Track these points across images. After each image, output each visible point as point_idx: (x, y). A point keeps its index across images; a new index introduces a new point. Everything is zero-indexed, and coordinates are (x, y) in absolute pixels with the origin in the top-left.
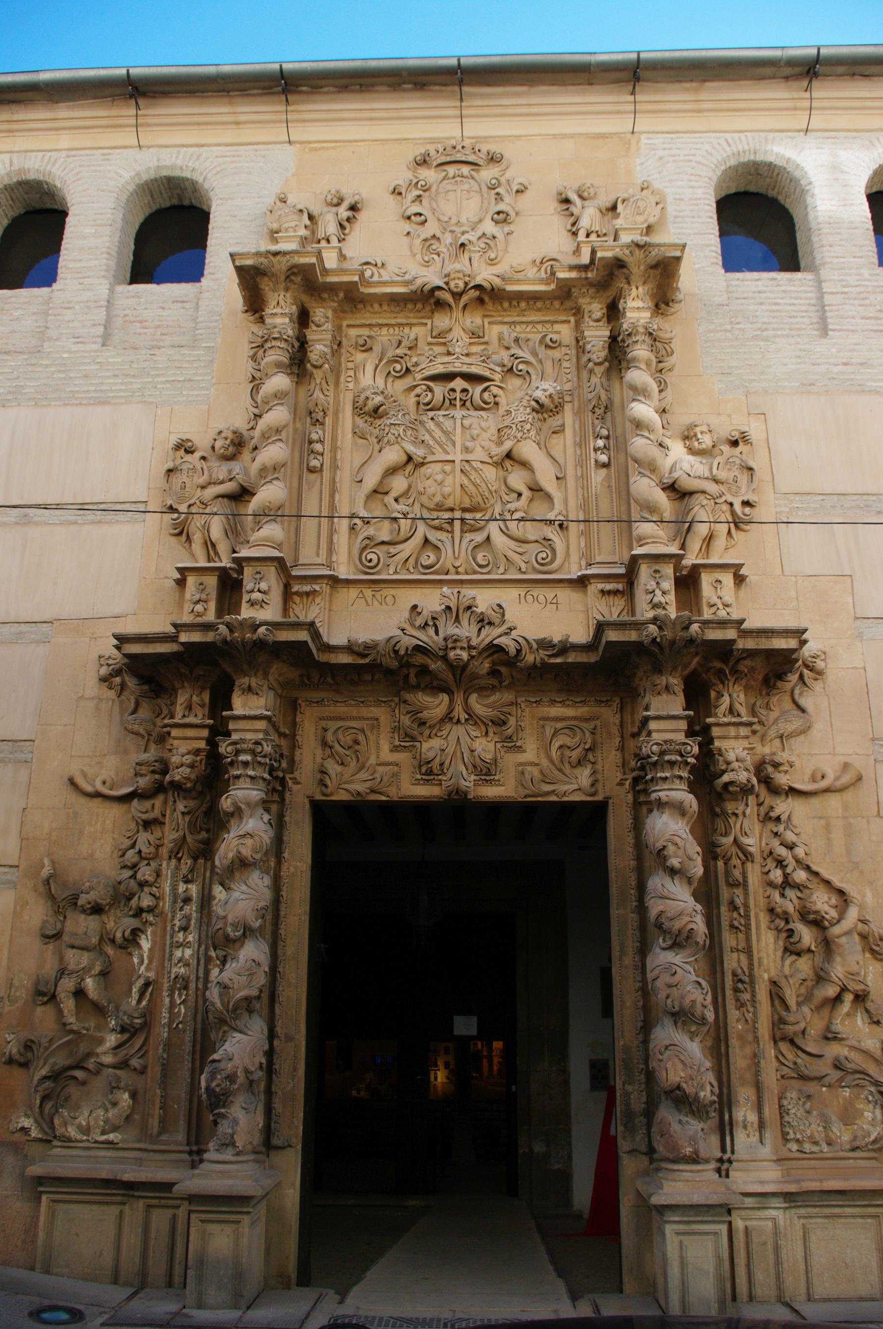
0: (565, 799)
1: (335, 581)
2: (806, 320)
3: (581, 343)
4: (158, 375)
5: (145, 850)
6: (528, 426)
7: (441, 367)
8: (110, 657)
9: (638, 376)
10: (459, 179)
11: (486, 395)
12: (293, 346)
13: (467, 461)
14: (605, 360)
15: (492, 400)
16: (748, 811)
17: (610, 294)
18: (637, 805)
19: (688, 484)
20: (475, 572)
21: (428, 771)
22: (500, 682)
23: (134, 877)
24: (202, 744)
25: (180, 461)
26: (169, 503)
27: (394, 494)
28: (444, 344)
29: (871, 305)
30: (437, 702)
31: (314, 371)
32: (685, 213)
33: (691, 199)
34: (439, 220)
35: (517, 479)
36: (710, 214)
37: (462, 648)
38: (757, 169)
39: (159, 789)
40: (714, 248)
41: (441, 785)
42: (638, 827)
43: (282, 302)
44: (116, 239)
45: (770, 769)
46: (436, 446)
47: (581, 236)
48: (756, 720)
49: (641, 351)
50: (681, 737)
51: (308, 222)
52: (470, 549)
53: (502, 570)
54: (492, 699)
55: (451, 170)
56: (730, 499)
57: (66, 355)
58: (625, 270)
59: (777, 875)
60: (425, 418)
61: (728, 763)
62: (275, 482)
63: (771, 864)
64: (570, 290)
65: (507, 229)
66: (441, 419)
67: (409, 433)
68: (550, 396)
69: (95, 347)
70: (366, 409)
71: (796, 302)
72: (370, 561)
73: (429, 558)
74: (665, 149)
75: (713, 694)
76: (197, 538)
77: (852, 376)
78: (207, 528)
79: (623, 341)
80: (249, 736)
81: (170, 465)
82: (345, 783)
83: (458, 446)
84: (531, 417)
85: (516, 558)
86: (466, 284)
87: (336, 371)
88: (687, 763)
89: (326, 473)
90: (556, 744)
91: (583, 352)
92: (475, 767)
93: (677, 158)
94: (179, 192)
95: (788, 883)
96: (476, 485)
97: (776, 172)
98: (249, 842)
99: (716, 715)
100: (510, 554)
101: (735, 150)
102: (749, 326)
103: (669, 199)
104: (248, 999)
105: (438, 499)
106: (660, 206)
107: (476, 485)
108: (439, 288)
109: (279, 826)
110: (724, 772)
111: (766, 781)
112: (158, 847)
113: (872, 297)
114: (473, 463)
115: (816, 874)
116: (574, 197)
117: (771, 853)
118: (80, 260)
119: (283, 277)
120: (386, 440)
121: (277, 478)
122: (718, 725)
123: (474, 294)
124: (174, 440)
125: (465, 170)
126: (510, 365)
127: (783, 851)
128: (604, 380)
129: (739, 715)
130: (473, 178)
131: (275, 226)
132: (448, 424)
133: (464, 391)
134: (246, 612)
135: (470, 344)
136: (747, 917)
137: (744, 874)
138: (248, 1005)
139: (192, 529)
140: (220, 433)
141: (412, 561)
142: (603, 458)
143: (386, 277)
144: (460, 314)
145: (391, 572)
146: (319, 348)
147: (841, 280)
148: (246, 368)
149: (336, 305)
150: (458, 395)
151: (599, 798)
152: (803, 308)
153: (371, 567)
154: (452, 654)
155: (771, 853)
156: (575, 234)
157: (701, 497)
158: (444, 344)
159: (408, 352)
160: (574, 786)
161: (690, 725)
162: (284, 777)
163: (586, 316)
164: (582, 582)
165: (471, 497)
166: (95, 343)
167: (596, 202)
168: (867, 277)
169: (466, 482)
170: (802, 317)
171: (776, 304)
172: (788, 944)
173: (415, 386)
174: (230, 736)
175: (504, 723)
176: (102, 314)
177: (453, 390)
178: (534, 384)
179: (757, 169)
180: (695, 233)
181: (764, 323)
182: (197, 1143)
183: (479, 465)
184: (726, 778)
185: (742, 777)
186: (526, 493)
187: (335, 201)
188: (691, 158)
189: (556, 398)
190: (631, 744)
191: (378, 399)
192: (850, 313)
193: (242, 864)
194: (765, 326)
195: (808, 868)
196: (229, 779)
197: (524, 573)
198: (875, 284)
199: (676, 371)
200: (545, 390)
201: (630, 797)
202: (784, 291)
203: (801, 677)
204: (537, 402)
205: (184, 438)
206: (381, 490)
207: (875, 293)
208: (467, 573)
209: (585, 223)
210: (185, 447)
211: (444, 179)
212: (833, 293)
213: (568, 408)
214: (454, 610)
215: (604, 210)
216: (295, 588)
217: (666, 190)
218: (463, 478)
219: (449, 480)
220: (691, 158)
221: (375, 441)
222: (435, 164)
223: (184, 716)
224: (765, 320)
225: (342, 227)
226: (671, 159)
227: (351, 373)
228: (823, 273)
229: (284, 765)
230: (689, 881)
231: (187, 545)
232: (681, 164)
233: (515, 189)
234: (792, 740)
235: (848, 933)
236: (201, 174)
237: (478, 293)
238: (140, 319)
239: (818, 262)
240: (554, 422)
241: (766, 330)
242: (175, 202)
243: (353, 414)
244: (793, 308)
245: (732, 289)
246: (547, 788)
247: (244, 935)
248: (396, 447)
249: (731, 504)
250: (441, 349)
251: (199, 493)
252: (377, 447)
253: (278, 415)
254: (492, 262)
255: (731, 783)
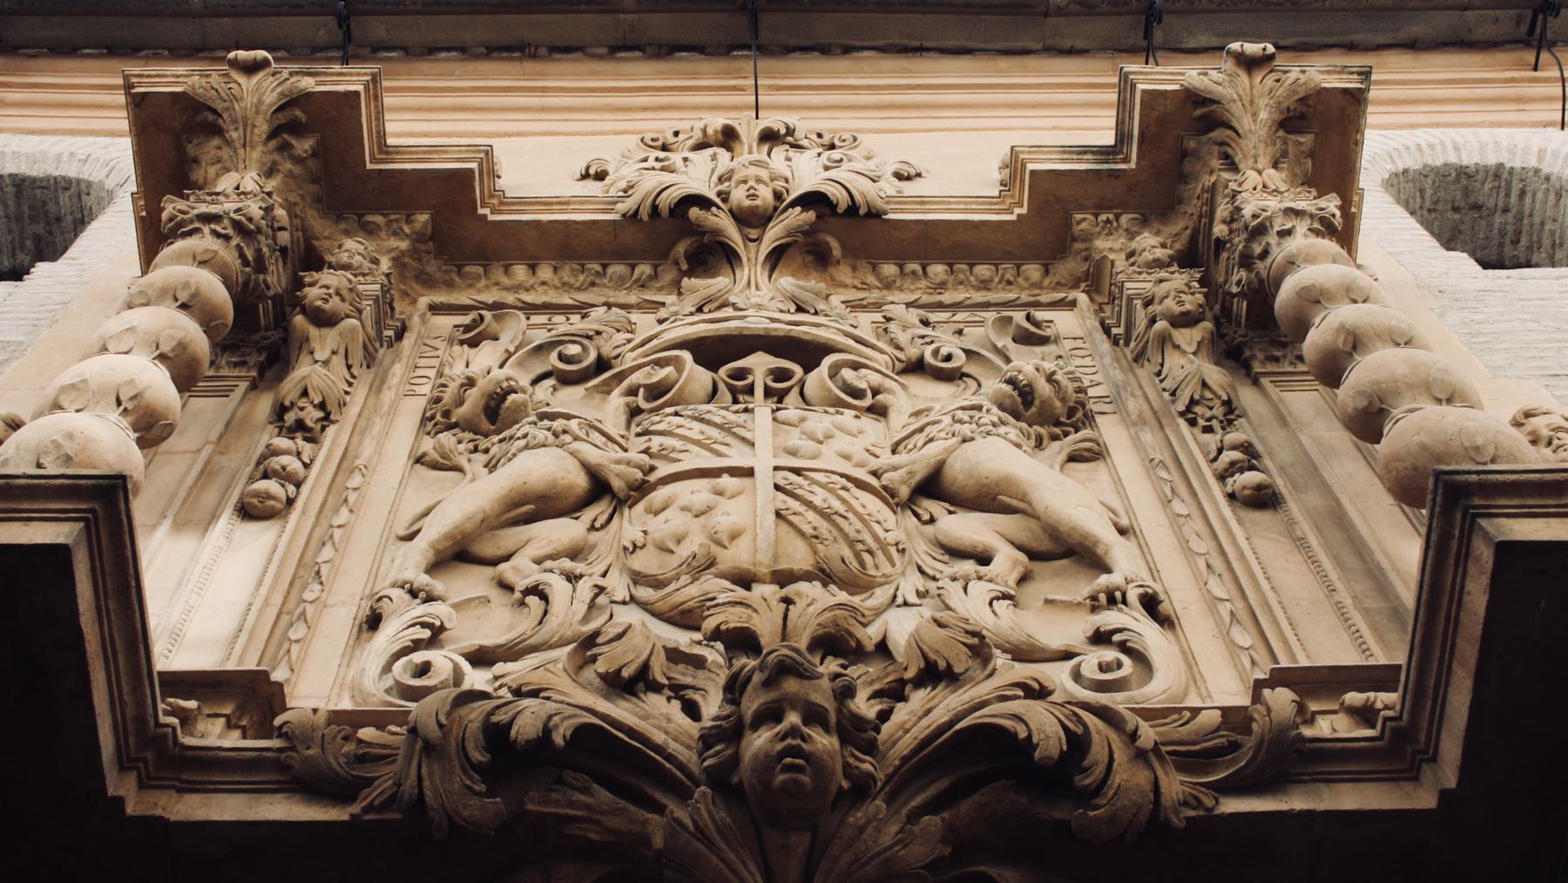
31: (313, 332)
38: (1467, 192)
58: (1220, 134)
86: (778, 196)
94: (40, 229)
97: (1516, 187)
105: (694, 544)
119: (262, 128)
123: (797, 217)
144: (761, 276)
149: (404, 245)
165: (813, 539)
179: (1467, 192)
237: (811, 215)
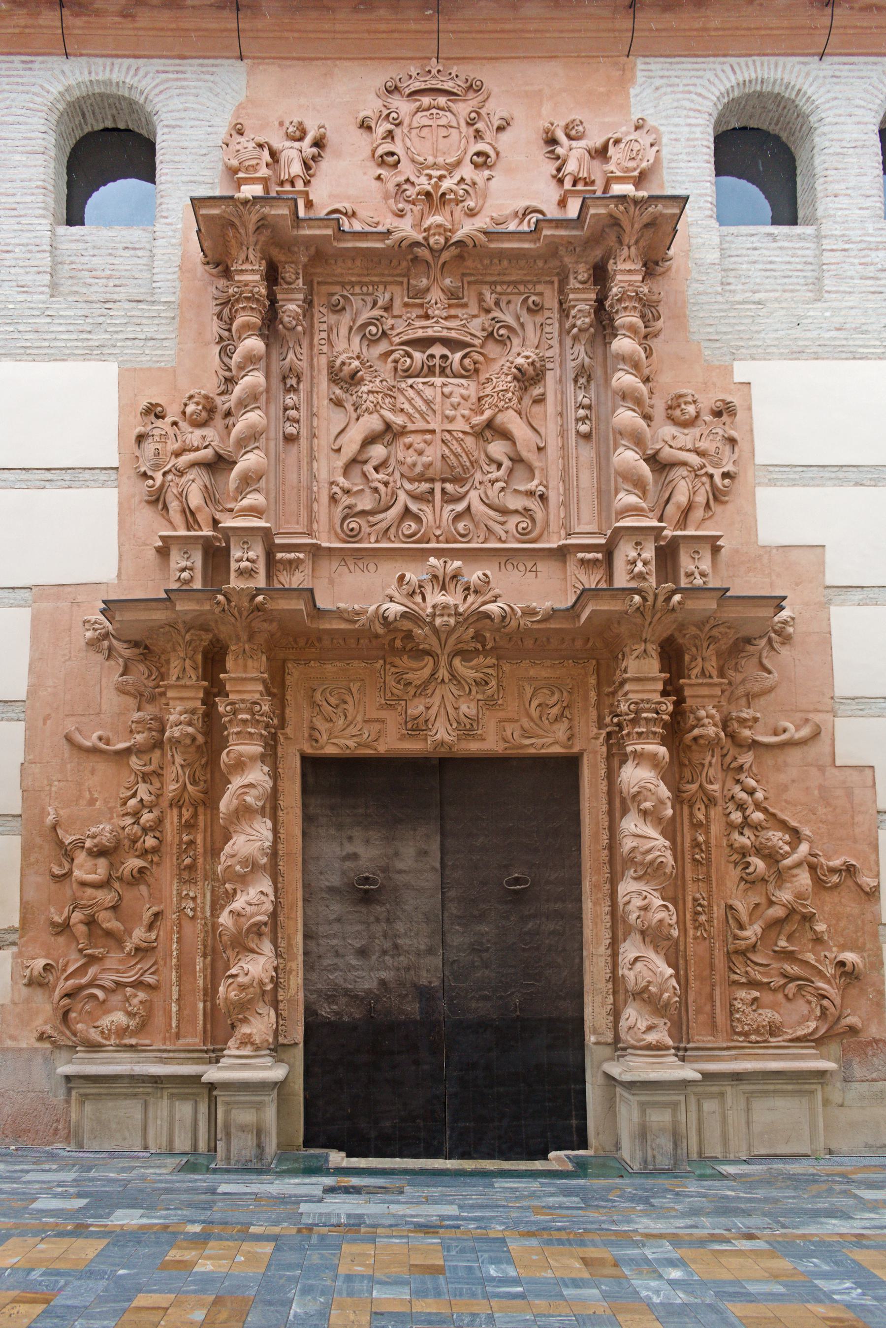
0: (543, 751)
1: (316, 551)
2: (802, 281)
3: (564, 306)
4: (117, 332)
5: (146, 798)
6: (510, 395)
7: (420, 331)
8: (96, 622)
9: (623, 344)
10: (434, 111)
11: (467, 361)
12: (264, 306)
13: (449, 431)
14: (591, 326)
15: (472, 367)
16: (714, 761)
17: (597, 254)
18: (610, 756)
19: (667, 453)
20: (456, 542)
21: (417, 728)
22: (484, 646)
23: (137, 822)
24: (198, 704)
25: (151, 427)
26: (142, 469)
27: (374, 462)
28: (421, 306)
29: (872, 264)
30: (422, 664)
32: (680, 157)
33: (688, 140)
34: (413, 161)
35: (497, 449)
36: (707, 157)
37: (449, 615)
39: (158, 744)
40: (710, 199)
41: (426, 739)
42: (611, 776)
43: (251, 257)
44: (51, 171)
45: (736, 725)
46: (417, 415)
47: (568, 185)
48: (726, 681)
49: (627, 318)
50: (657, 697)
51: (269, 159)
52: (451, 518)
53: (482, 539)
54: (474, 662)
55: (426, 100)
56: (711, 470)
57: (11, 306)
59: (736, 817)
60: (403, 385)
61: (699, 719)
62: (256, 451)
63: (731, 806)
64: (557, 248)
65: (487, 173)
66: (421, 386)
67: (387, 400)
68: (533, 363)
69: (43, 297)
70: (342, 374)
71: (792, 260)
72: (352, 530)
73: (410, 526)
74: (662, 77)
75: (687, 658)
76: (174, 506)
77: (844, 342)
78: (182, 496)
79: (612, 306)
80: (246, 696)
81: (140, 429)
82: (336, 737)
83: (439, 412)
84: (512, 385)
85: (497, 528)
86: (447, 240)
87: (310, 331)
88: (662, 720)
89: (303, 441)
90: (534, 704)
91: (567, 316)
92: (459, 723)
93: (676, 89)
95: (746, 822)
96: (457, 456)
98: (253, 792)
99: (689, 677)
100: (491, 524)
101: (741, 80)
102: (740, 287)
103: (665, 140)
104: (258, 925)
106: (655, 148)
107: (457, 456)
108: (417, 244)
109: (275, 776)
110: (694, 727)
111: (732, 736)
112: (158, 796)
113: (873, 254)
114: (454, 433)
115: (774, 815)
116: (561, 136)
117: (733, 797)
118: (14, 195)
120: (364, 407)
121: (257, 447)
122: (691, 685)
123: (454, 251)
124: (143, 403)
125: (442, 100)
126: (490, 329)
127: (744, 796)
128: (588, 346)
129: (710, 677)
130: (450, 111)
131: (235, 163)
132: (428, 392)
133: (444, 357)
134: (235, 583)
135: (450, 306)
136: (709, 852)
137: (707, 816)
138: (257, 930)
139: (170, 497)
140: (191, 397)
141: (393, 530)
142: (584, 428)
143: (357, 227)
145: (373, 540)
146: (291, 308)
147: (843, 235)
148: (215, 328)
150: (437, 361)
151: (576, 750)
152: (799, 267)
153: (353, 535)
154: (438, 621)
155: (733, 797)
156: (561, 181)
157: (683, 471)
158: (421, 306)
159: (385, 314)
160: (551, 742)
161: (665, 684)
162: (276, 733)
163: (571, 277)
164: (562, 553)
166: (42, 293)
167: (582, 143)
168: (871, 231)
169: (447, 452)
170: (797, 277)
171: (771, 262)
172: (744, 875)
173: (392, 352)
174: (227, 696)
175: (487, 683)
176: (46, 261)
177: (432, 356)
178: (515, 350)
180: (688, 166)
181: (756, 284)
182: (214, 1041)
183: (461, 435)
184: (696, 732)
185: (711, 731)
186: (507, 463)
187: (298, 134)
188: (692, 88)
189: (538, 365)
190: (607, 701)
191: (356, 363)
192: (849, 274)
193: (243, 812)
194: (756, 288)
195: (765, 811)
196: (228, 735)
197: (504, 542)
198: (879, 239)
199: (662, 336)
200: (527, 357)
201: (604, 749)
202: (781, 248)
203: (770, 641)
204: (519, 370)
205: (154, 402)
206: (360, 458)
207: (877, 249)
208: (447, 542)
209: (571, 167)
210: (154, 412)
211: (418, 110)
212: (832, 250)
213: (549, 375)
214: (441, 579)
215: (593, 153)
216: (279, 556)
217: (662, 129)
218: (445, 448)
219: (429, 451)
220: (692, 88)
221: (352, 408)
222: (407, 91)
223: (178, 678)
224: (758, 280)
225: (307, 167)
226: (669, 89)
227: (324, 335)
228: (827, 227)
229: (276, 721)
230: (660, 820)
231: (164, 512)
232: (680, 96)
233: (496, 123)
234: (756, 700)
235: (798, 865)
236: (142, 93)
238: (89, 266)
239: (820, 213)
240: (536, 391)
241: (758, 291)
242: (109, 124)
243: (329, 380)
244: (788, 266)
245: (725, 246)
246: (527, 742)
247: (252, 871)
248: (375, 416)
249: (711, 476)
250: (420, 312)
251: (173, 461)
252: (354, 416)
253: (254, 379)
254: (472, 213)
255: (701, 736)
